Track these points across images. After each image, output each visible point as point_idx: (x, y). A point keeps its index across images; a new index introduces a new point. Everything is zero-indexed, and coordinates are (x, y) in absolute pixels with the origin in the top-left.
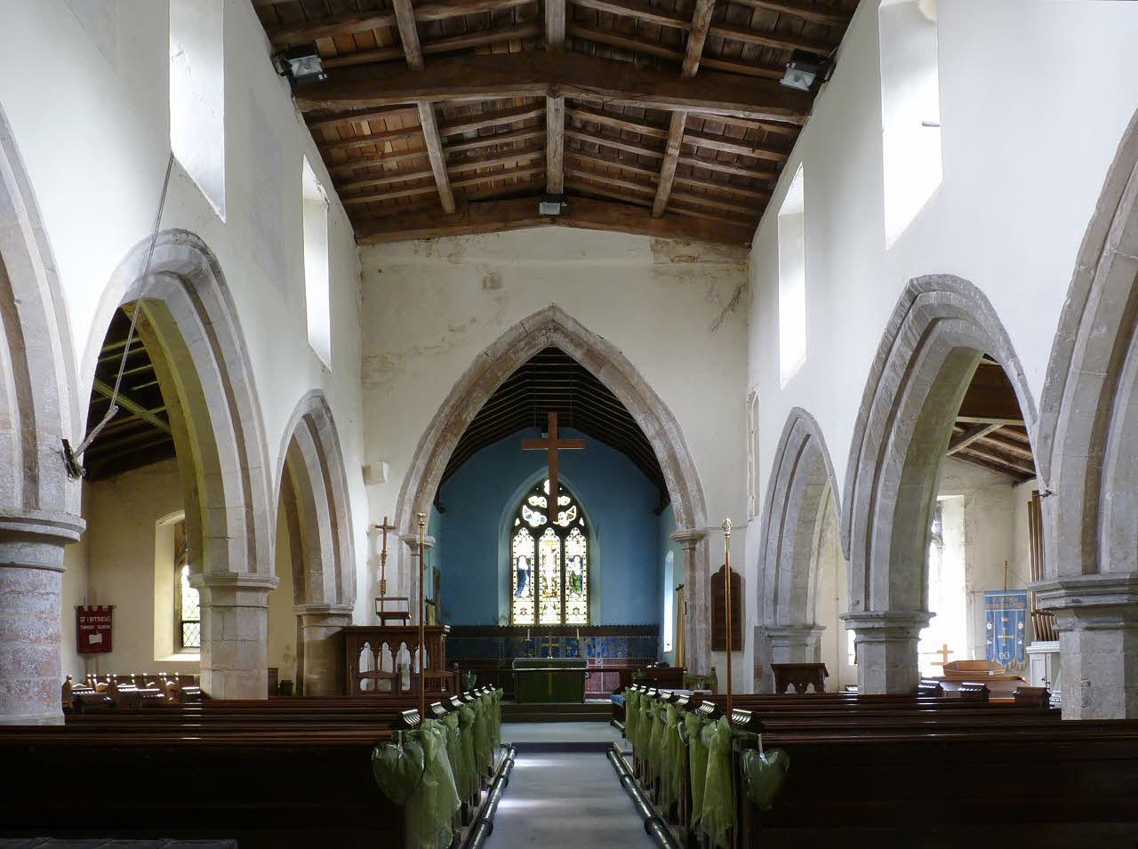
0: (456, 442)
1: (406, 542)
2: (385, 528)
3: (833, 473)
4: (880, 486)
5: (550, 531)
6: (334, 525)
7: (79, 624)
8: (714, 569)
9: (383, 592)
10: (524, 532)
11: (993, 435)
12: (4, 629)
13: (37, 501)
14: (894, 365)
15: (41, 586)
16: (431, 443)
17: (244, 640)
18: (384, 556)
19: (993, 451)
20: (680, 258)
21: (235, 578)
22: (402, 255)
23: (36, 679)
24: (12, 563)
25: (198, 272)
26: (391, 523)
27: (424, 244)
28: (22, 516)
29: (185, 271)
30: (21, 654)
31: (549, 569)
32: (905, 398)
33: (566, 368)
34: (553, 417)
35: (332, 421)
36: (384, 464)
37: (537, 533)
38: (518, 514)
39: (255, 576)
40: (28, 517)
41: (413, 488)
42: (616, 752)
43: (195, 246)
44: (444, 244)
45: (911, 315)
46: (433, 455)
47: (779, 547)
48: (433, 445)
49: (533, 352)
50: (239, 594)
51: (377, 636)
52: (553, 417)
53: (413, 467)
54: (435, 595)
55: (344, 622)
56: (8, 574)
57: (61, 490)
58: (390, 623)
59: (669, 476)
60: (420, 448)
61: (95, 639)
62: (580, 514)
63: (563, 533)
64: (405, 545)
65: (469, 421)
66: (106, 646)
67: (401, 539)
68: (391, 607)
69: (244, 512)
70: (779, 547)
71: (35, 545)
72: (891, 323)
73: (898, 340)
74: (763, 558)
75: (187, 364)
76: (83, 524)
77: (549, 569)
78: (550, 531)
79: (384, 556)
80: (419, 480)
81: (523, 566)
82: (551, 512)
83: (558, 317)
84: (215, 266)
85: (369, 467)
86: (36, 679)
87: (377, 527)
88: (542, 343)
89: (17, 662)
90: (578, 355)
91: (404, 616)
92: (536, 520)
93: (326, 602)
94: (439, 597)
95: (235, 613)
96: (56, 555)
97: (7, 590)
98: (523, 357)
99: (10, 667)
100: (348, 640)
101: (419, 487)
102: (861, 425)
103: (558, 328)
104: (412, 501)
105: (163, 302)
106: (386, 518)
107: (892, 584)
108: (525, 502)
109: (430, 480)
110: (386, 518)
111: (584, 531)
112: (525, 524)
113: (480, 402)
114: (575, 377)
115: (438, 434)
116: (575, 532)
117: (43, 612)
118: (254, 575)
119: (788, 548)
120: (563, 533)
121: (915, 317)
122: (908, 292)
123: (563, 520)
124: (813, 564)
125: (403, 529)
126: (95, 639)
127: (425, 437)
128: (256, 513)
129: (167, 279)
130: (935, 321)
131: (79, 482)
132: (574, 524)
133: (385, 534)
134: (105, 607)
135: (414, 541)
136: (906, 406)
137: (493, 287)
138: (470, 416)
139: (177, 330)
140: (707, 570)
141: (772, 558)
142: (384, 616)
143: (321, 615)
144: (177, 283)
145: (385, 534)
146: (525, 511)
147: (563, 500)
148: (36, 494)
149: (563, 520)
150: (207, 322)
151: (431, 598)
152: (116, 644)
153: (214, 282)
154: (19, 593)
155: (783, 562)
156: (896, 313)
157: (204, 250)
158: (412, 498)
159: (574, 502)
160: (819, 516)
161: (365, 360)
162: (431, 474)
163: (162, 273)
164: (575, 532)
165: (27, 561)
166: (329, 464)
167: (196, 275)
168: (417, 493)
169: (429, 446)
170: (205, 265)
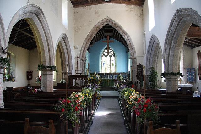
0: (90, 41)
2: (78, 57)
3: (161, 48)
4: (171, 50)
5: (108, 56)
7: (27, 75)
8: (138, 64)
9: (77, 69)
10: (104, 56)
11: (189, 40)
14: (173, 27)
18: (77, 62)
19: (188, 42)
20: (130, 8)
22: (81, 9)
25: (38, 12)
26: (79, 56)
27: (85, 7)
29: (35, 12)
31: (108, 62)
32: (176, 33)
33: (110, 28)
34: (108, 36)
35: (67, 38)
37: (106, 56)
38: (103, 53)
42: (119, 99)
43: (37, 7)
44: (88, 7)
45: (177, 17)
47: (150, 61)
49: (104, 25)
51: (76, 77)
52: (108, 36)
54: (88, 68)
55: (70, 75)
58: (78, 75)
59: (129, 47)
60: (84, 43)
61: (30, 77)
62: (114, 53)
63: (111, 56)
65: (93, 38)
66: (31, 78)
67: (81, 59)
68: (79, 72)
70: (150, 61)
72: (173, 18)
73: (174, 22)
74: (147, 62)
75: (37, 29)
77: (108, 62)
78: (108, 56)
81: (104, 62)
82: (108, 53)
83: (109, 19)
84: (42, 11)
88: (106, 23)
90: (112, 25)
91: (81, 73)
92: (106, 54)
94: (89, 68)
98: (103, 26)
100: (71, 78)
102: (167, 38)
103: (109, 20)
105: (32, 18)
108: (104, 51)
111: (114, 56)
112: (104, 55)
113: (95, 34)
114: (113, 29)
116: (113, 56)
119: (151, 61)
120: (111, 56)
121: (178, 17)
122: (177, 12)
123: (111, 54)
124: (156, 64)
125: (81, 57)
126: (30, 77)
129: (32, 14)
130: (182, 18)
132: (113, 55)
134: (31, 71)
136: (176, 35)
137: (97, 14)
138: (93, 37)
139: (35, 24)
140: (136, 64)
141: (148, 62)
142: (77, 73)
143: (66, 73)
144: (34, 15)
146: (104, 52)
147: (110, 51)
149: (111, 54)
150: (41, 22)
151: (88, 68)
152: (33, 78)
153: (42, 14)
155: (151, 63)
156: (174, 16)
157: (39, 8)
159: (112, 51)
160: (157, 54)
161: (75, 28)
163: (31, 13)
164: (113, 56)
167: (38, 13)
169: (86, 42)
170: (39, 11)
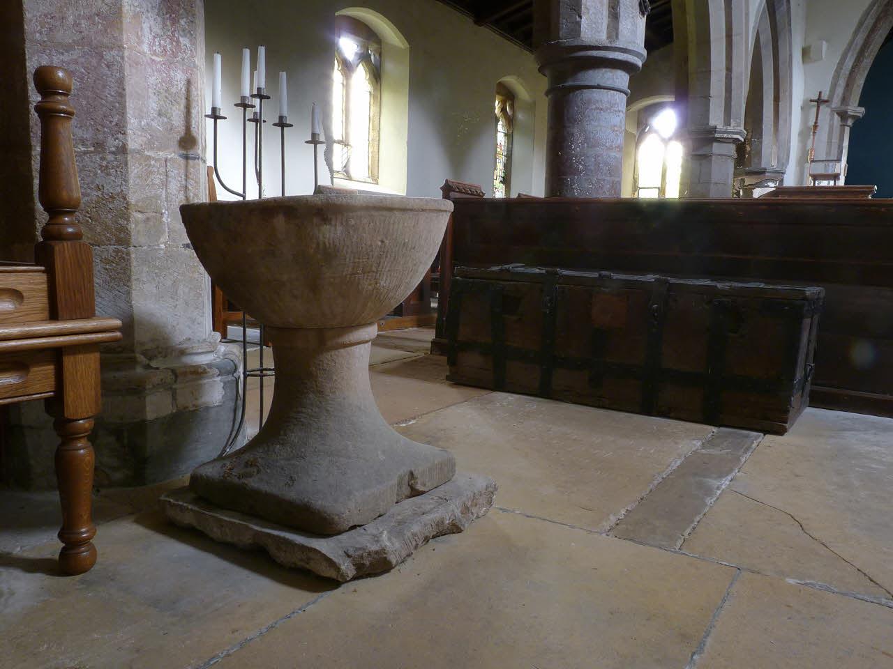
1: (837, 113)
2: (820, 101)
6: (777, 99)
12: (590, 138)
13: (617, 34)
15: (615, 104)
16: (872, 19)
17: (716, 183)
18: (815, 126)
21: (714, 129)
23: (608, 178)
24: (598, 85)
28: (609, 45)
30: (599, 158)
36: (824, 42)
39: (730, 129)
40: (613, 45)
41: (849, 63)
46: (873, 30)
48: (874, 20)
50: (715, 144)
53: (851, 42)
56: (595, 95)
57: (634, 24)
60: (861, 24)
64: (836, 116)
67: (833, 111)
69: (725, 74)
71: (614, 71)
76: (645, 53)
79: (815, 126)
80: (855, 56)
85: (810, 47)
86: (608, 178)
87: (811, 101)
89: (597, 164)
93: (763, 166)
95: (711, 160)
96: (269, 373)
97: (594, 107)
99: (593, 168)
101: (855, 62)
104: (847, 76)
106: (820, 93)
107: (371, 384)
109: (866, 54)
110: (820, 93)
115: (880, 9)
117: (615, 126)
118: (729, 128)
125: (836, 102)
127: (867, 13)
128: (734, 74)
131: (644, 19)
133: (818, 107)
135: (846, 112)
145: (818, 107)
148: (617, 29)
154: (602, 109)
158: (848, 73)
162: (869, 47)
165: (609, 84)
166: (780, 43)
168: (853, 68)
169: (870, 22)
